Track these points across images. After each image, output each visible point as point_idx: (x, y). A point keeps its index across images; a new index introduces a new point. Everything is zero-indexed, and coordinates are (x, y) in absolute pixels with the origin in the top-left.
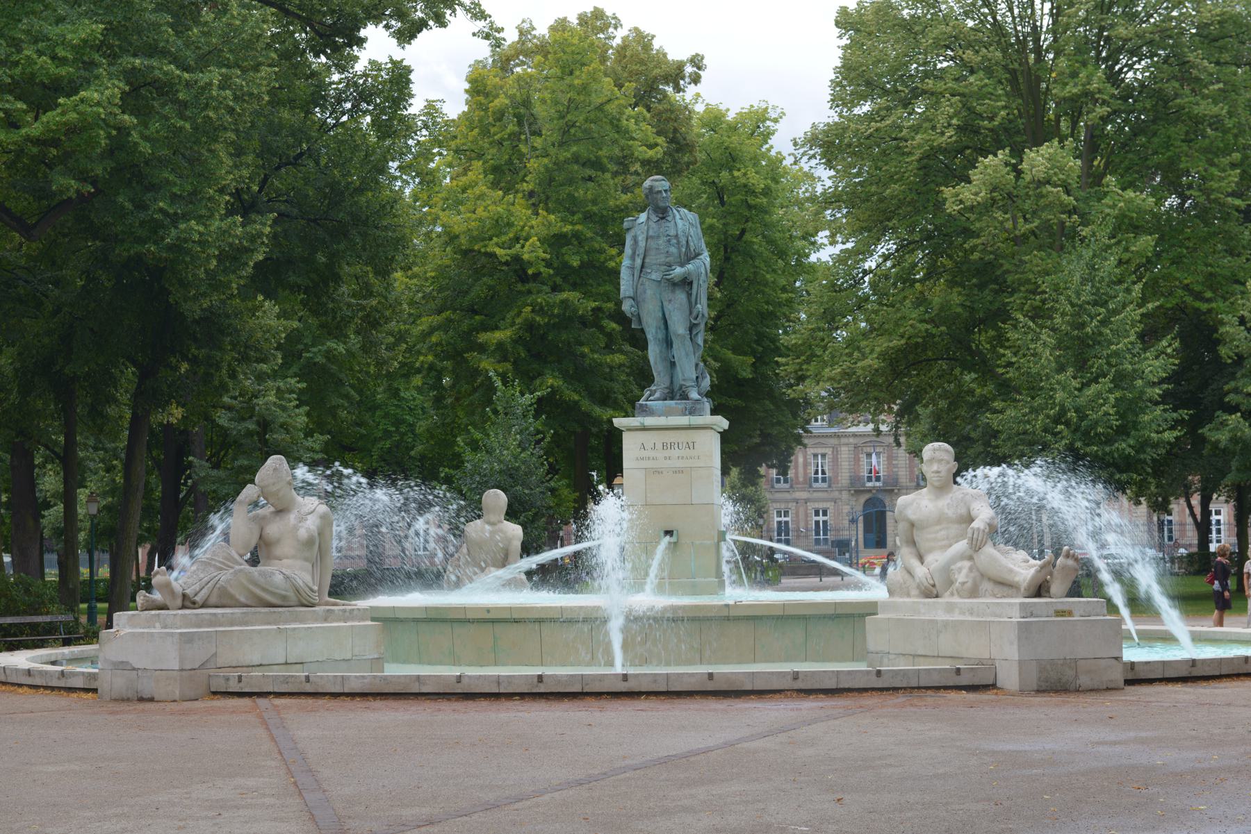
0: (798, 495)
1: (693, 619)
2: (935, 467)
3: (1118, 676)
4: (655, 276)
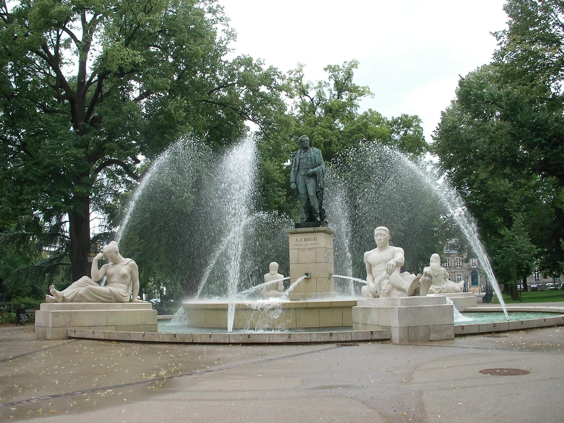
0: (452, 271)
1: (202, 309)
2: (379, 238)
3: (451, 333)
4: (303, 173)
